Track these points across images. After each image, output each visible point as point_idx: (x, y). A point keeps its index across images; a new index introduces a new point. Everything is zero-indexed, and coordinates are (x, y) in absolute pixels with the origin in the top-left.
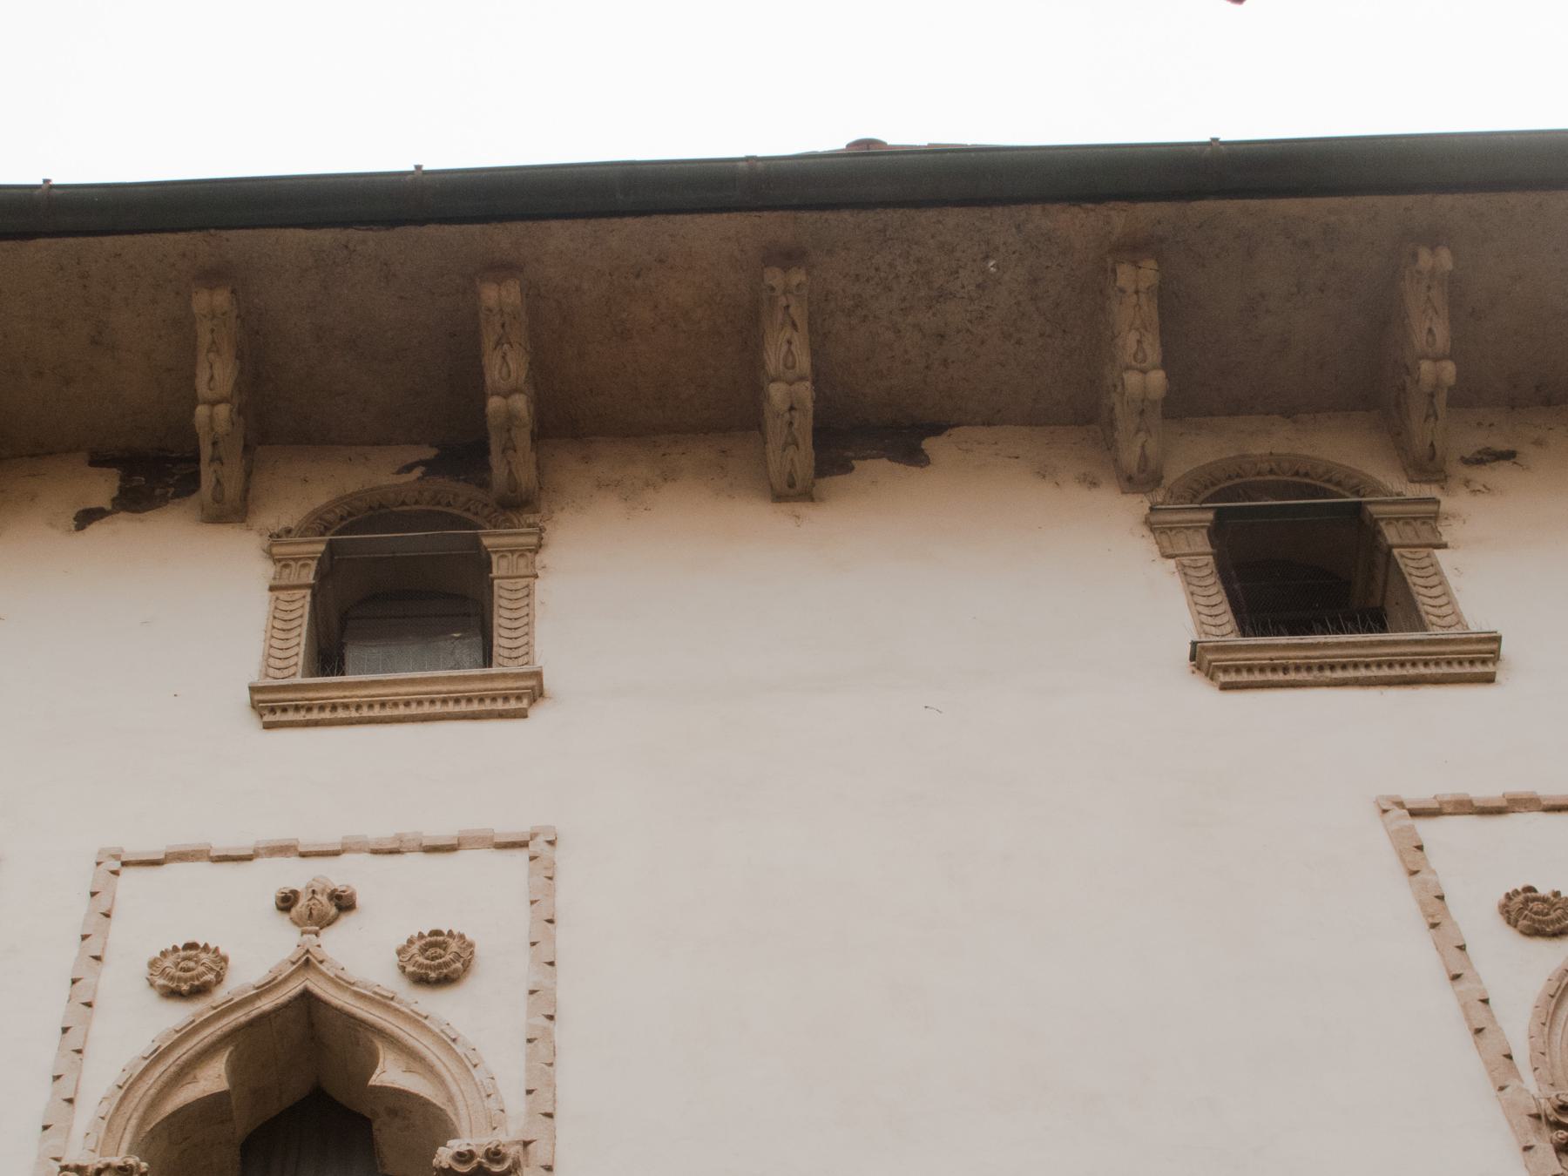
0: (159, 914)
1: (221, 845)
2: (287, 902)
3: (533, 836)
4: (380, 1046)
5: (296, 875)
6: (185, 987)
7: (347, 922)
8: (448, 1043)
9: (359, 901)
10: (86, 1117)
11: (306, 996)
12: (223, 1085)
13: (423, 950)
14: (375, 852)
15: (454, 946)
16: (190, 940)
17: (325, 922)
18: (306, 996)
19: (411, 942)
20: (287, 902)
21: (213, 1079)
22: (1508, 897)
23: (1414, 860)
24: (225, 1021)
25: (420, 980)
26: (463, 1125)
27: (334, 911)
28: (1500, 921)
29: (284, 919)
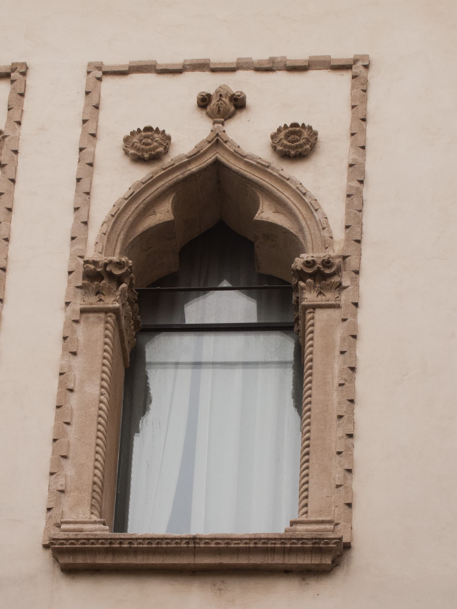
8: (301, 195)
10: (94, 233)
15: (305, 134)
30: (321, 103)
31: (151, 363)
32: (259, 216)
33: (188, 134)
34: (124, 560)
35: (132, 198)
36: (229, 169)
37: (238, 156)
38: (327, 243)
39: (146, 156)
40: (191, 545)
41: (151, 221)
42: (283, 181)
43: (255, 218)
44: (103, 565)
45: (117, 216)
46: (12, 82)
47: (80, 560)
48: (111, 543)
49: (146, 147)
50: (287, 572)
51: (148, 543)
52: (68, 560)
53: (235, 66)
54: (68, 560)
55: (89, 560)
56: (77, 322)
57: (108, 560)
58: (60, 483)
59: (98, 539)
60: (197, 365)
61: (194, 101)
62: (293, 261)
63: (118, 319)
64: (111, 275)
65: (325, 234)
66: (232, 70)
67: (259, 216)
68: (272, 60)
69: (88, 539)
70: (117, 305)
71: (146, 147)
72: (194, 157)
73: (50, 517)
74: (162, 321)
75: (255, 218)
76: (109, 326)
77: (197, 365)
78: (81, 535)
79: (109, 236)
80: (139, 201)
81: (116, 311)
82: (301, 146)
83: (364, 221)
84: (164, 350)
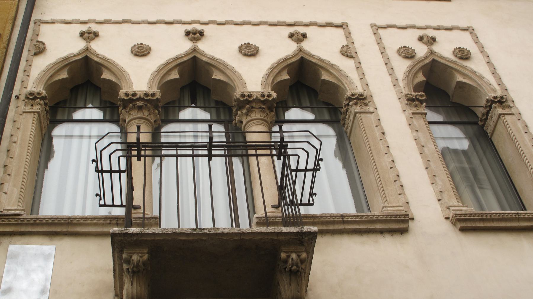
0: (394, 40)
1: (167, 19)
2: (291, 36)
3: (343, 25)
4: (214, 70)
5: (190, 28)
6: (409, 56)
7: (97, 39)
8: (474, 73)
9: (100, 34)
10: (401, 84)
11: (434, 60)
12: (178, 76)
13: (138, 48)
14: (434, 29)
15: (466, 51)
16: (405, 45)
17: (301, 41)
18: (434, 60)
19: (135, 45)
20: (82, 34)
21: (64, 75)
22: (132, 48)
23: (379, 41)
24: (419, 65)
25: (461, 58)
26: (124, 88)
27: (94, 37)
28: (341, 55)
29: (187, 38)
30: (465, 41)
31: (55, 136)
32: (103, 76)
33: (421, 50)
34: (331, 227)
35: (410, 71)
36: (439, 62)
37: (441, 57)
38: (494, 90)
39: (409, 56)
40: (517, 217)
41: (279, 79)
42: (465, 67)
43: (102, 77)
44: (478, 227)
45: (407, 78)
46: (344, 29)
47: (469, 224)
48: (482, 216)
49: (407, 53)
50: (382, 232)
51: (386, 218)
52: (464, 225)
53: (224, 23)
54: (464, 225)
55: (473, 224)
56: (412, 118)
57: (481, 225)
58: (439, 188)
59: (476, 214)
60: (81, 137)
61: (184, 33)
62: (118, 95)
63: (39, 116)
64: (418, 100)
65: (491, 86)
66: (425, 29)
67: (103, 76)
68: (278, 22)
69: (471, 214)
70: (39, 110)
71: (407, 53)
72: (426, 57)
73: (441, 204)
74: (171, 118)
75: (102, 77)
76: (35, 119)
77: (81, 137)
78: (463, 212)
79: (39, 80)
80: (411, 74)
81: (38, 113)
82: (252, 51)
83: (504, 82)
84: (59, 130)
